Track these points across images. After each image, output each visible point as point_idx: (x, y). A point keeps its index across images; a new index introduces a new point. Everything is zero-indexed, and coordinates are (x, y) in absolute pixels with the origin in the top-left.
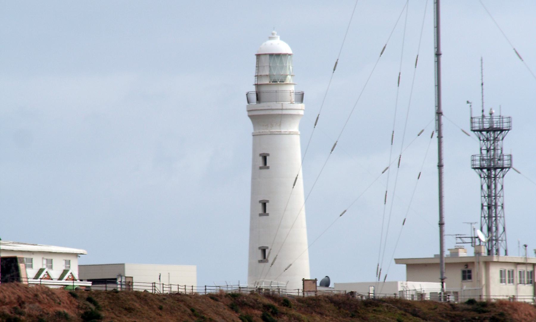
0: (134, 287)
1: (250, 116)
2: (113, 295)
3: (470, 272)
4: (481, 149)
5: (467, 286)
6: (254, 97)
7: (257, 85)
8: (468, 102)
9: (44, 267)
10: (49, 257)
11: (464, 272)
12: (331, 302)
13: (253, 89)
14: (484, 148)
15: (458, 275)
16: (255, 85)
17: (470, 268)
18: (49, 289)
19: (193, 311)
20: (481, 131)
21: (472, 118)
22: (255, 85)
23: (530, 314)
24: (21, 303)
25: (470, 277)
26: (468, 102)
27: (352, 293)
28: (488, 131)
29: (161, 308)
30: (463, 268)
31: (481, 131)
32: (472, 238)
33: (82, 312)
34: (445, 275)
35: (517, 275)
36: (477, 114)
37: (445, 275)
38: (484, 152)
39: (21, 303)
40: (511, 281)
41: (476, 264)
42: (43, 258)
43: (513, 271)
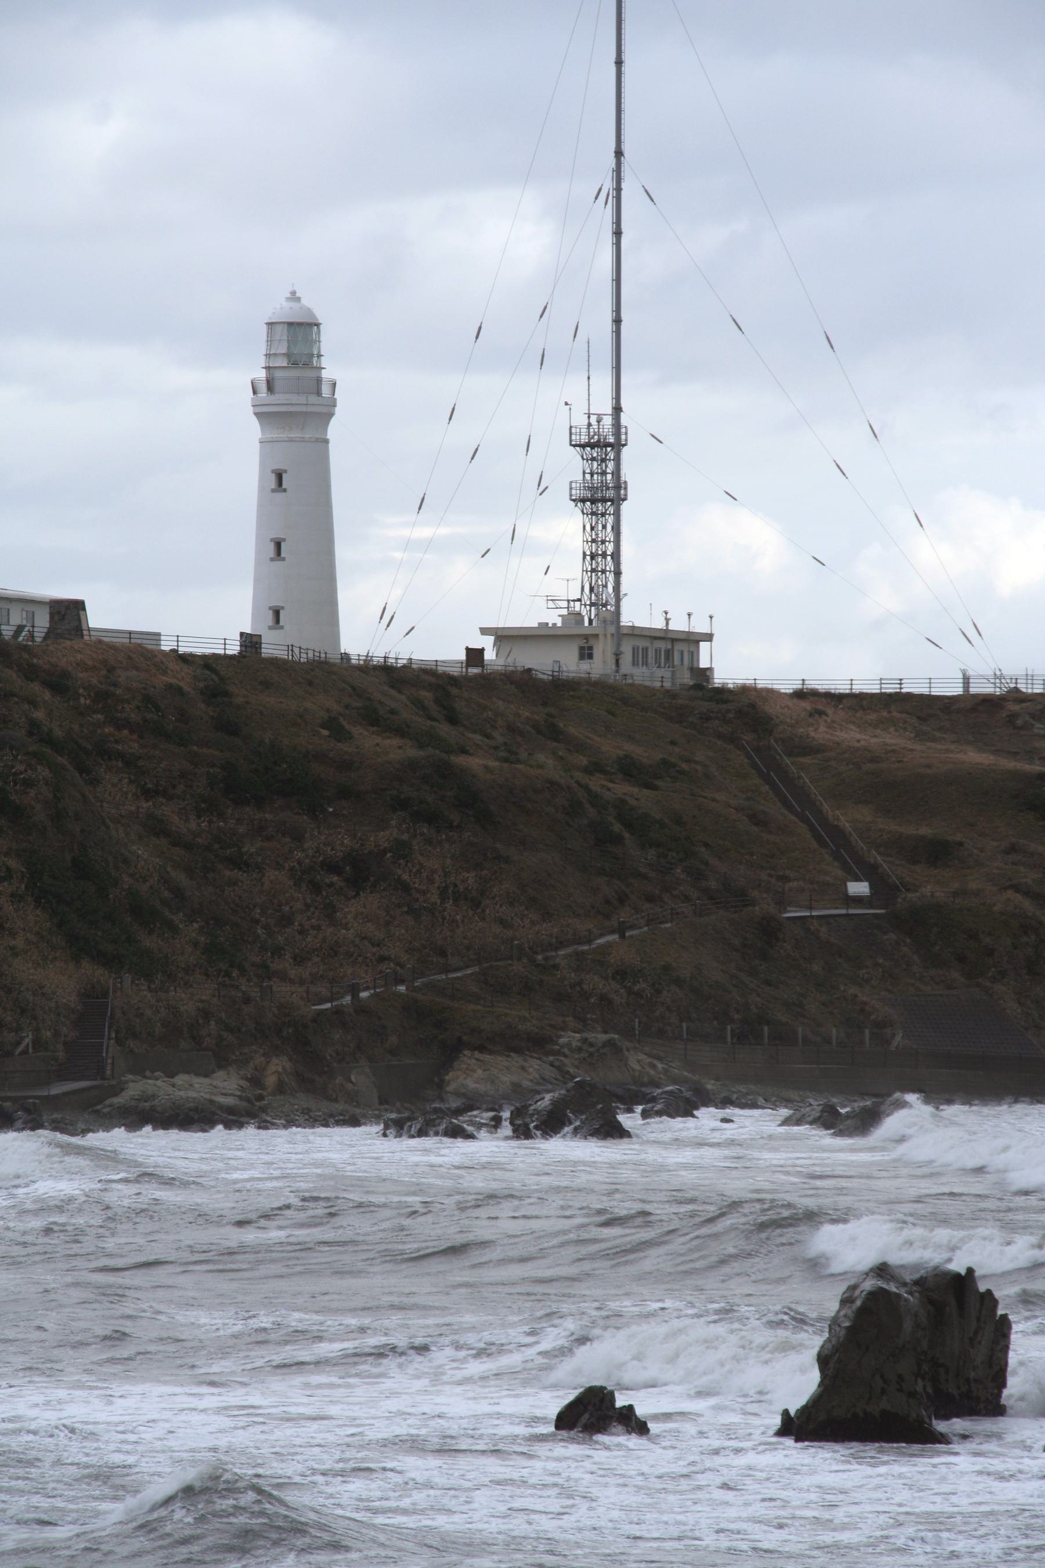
0: (263, 650)
1: (256, 414)
2: (239, 662)
3: (591, 648)
4: (584, 473)
5: (585, 666)
6: (263, 387)
7: (268, 368)
8: (566, 404)
9: (24, 623)
10: (30, 608)
11: (582, 648)
12: (511, 683)
13: (262, 374)
14: (588, 471)
15: (575, 653)
16: (265, 368)
17: (592, 642)
18: (146, 649)
19: (354, 689)
20: (583, 446)
21: (571, 427)
22: (265, 368)
23: (787, 706)
24: (111, 670)
25: (590, 656)
26: (566, 404)
27: (530, 670)
28: (592, 446)
29: (310, 683)
30: (582, 643)
31: (583, 446)
32: (568, 601)
33: (201, 685)
34: (621, 649)
35: (651, 653)
36: (581, 421)
37: (621, 649)
38: (588, 477)
39: (111, 670)
40: (645, 663)
41: (601, 637)
42: (23, 610)
43: (647, 649)
